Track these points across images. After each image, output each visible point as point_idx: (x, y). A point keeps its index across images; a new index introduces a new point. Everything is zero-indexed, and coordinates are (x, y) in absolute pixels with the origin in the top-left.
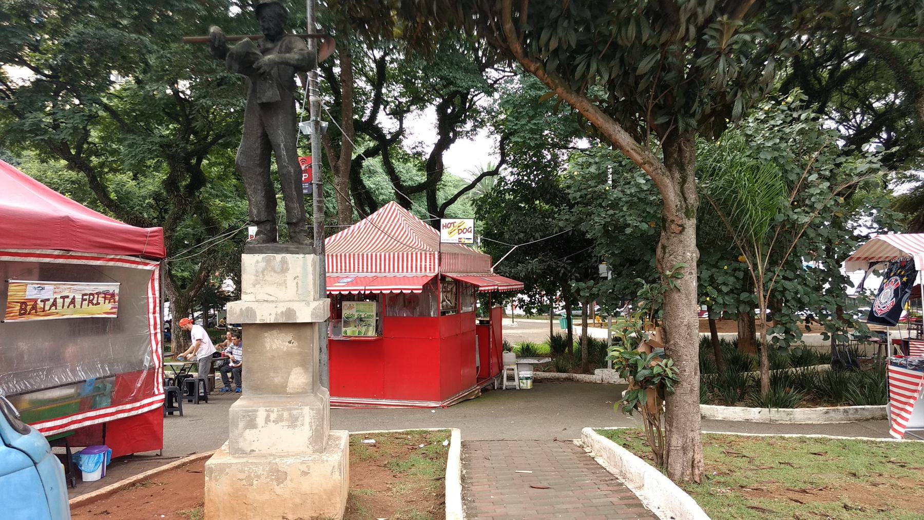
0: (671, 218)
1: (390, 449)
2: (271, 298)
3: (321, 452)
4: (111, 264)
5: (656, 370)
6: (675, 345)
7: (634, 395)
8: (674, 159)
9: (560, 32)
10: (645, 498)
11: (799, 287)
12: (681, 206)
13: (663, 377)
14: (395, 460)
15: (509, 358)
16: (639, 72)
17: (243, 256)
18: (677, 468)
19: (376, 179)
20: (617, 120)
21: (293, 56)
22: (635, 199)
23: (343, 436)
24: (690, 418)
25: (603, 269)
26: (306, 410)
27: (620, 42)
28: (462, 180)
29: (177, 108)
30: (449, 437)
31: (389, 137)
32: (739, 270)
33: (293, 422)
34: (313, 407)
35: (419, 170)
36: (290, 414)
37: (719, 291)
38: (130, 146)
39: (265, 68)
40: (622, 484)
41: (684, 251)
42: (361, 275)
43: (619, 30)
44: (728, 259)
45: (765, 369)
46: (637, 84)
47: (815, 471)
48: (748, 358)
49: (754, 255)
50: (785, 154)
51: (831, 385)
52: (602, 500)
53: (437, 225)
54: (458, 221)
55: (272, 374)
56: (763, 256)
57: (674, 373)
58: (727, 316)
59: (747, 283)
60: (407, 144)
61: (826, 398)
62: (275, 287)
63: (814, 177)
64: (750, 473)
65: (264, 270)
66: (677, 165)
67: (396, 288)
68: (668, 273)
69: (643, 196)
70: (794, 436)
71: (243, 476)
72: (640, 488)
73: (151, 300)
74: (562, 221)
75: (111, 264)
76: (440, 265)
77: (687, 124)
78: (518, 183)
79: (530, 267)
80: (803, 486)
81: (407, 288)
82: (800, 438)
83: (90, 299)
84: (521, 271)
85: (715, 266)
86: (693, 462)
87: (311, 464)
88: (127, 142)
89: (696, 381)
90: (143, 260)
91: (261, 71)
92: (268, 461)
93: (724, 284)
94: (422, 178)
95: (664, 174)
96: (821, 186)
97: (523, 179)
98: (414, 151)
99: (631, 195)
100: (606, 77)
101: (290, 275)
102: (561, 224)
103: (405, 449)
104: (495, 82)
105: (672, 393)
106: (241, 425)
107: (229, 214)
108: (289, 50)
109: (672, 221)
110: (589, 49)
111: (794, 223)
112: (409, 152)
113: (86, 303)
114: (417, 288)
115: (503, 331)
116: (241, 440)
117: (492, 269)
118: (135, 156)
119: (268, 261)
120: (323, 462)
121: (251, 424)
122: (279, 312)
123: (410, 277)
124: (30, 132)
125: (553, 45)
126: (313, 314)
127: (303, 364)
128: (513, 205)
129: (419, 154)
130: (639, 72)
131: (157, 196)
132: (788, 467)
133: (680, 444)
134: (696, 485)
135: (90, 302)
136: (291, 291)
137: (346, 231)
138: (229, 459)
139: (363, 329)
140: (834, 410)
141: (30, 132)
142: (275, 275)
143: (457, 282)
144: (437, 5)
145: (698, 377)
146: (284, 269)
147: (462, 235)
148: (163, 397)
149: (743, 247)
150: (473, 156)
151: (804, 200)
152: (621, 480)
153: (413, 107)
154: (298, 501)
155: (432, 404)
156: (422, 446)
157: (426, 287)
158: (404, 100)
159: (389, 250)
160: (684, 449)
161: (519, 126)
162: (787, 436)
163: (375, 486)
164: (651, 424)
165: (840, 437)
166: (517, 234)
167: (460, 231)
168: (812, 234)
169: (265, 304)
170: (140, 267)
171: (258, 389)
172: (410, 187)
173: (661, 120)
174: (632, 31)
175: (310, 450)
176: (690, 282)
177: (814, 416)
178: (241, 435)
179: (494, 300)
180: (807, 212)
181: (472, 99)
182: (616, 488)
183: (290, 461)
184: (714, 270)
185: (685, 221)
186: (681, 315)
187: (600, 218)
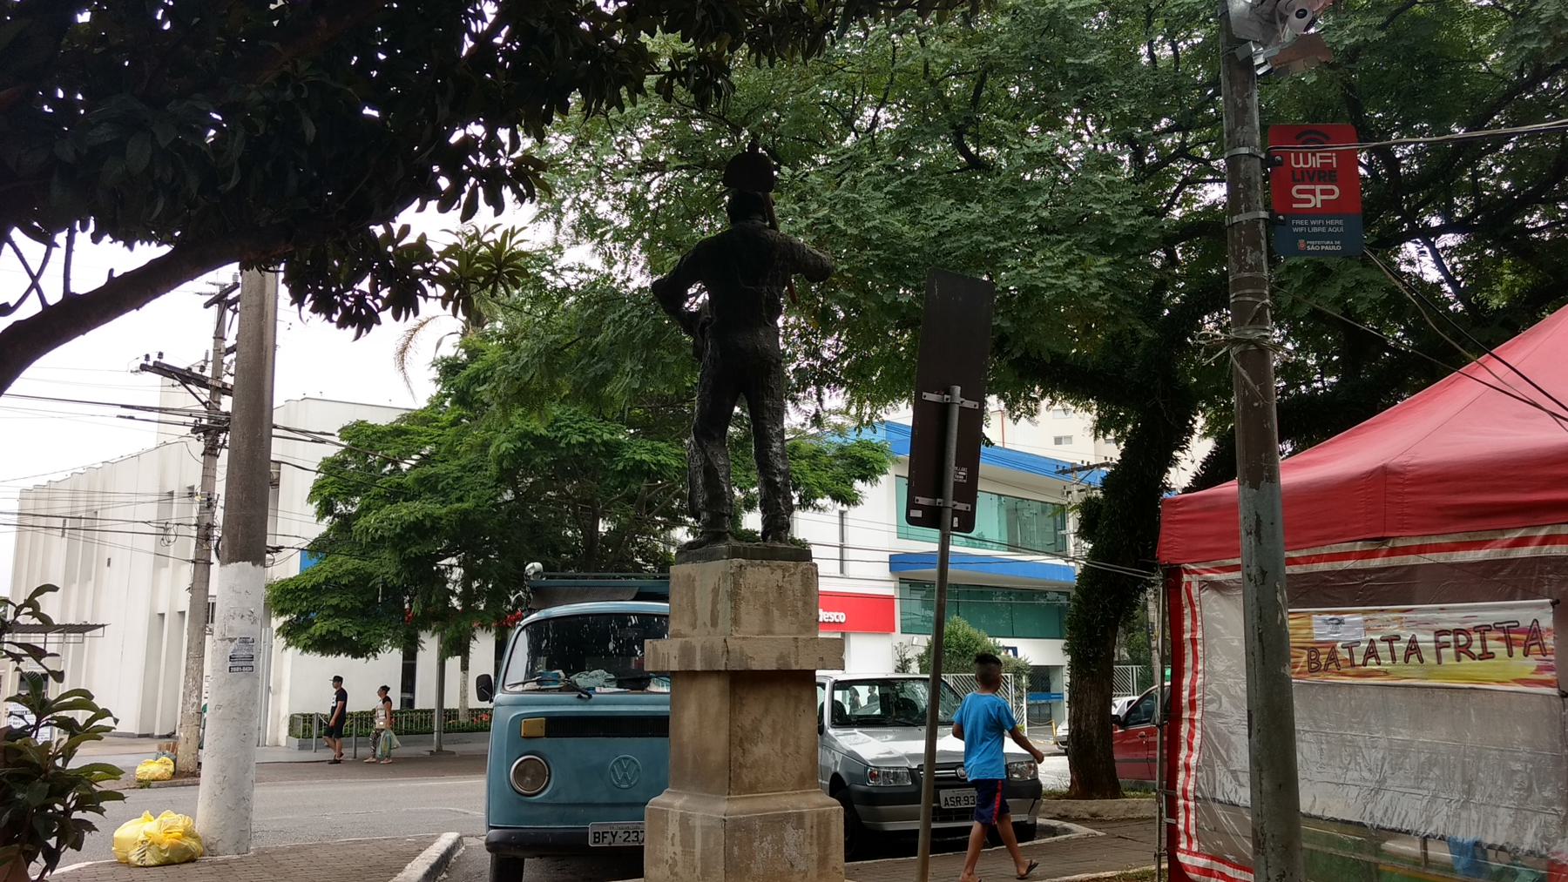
135: (1463, 650)
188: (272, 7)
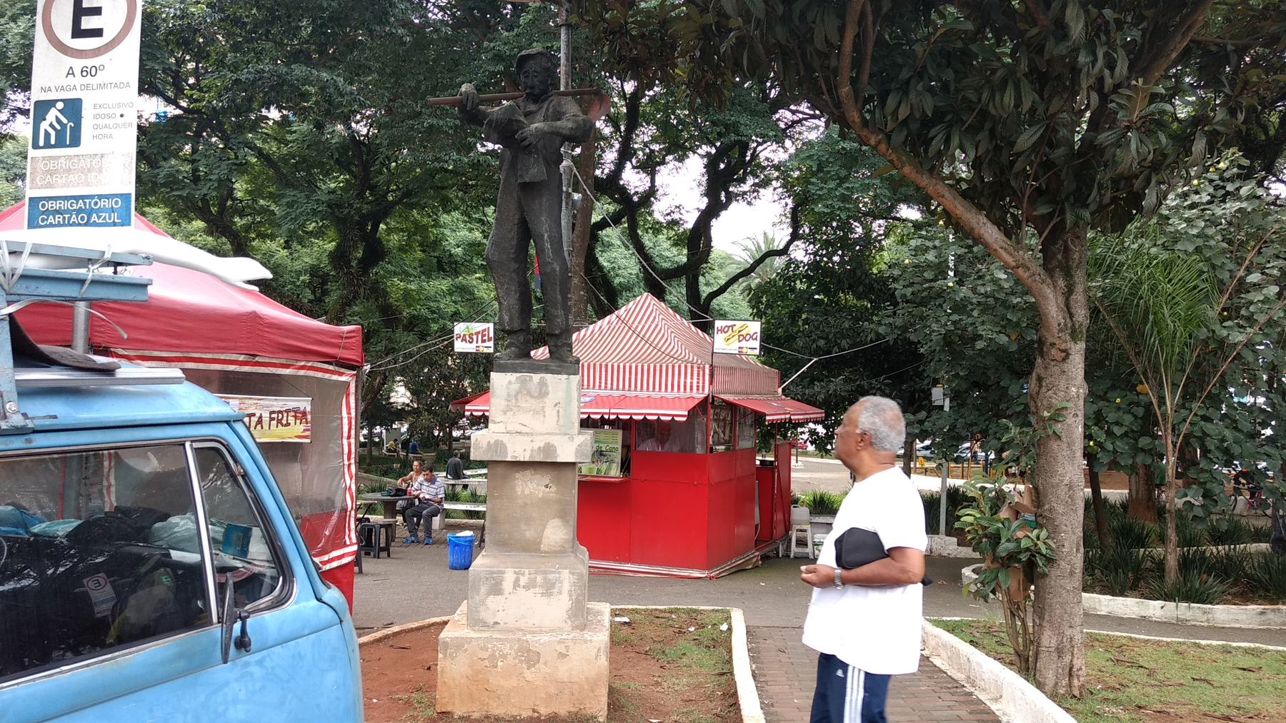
0: (1051, 340)
1: (650, 631)
2: (525, 430)
3: (582, 630)
4: (302, 373)
5: (1024, 544)
6: (1050, 510)
7: (993, 576)
8: (1056, 259)
9: (912, 96)
10: (1004, 714)
11: (1227, 433)
12: (1066, 325)
13: (1034, 552)
14: (659, 646)
15: (800, 514)
16: (1017, 148)
17: (493, 375)
18: (1050, 677)
19: (617, 257)
20: (980, 207)
21: (566, 124)
22: (991, 301)
23: (605, 608)
24: (1069, 610)
25: (937, 394)
26: (565, 574)
27: (993, 112)
28: (729, 257)
29: (357, 156)
30: (728, 619)
31: (635, 199)
32: (1138, 405)
33: (549, 589)
34: (573, 568)
35: (675, 244)
36: (545, 579)
37: (1109, 433)
38: (290, 205)
39: (531, 139)
40: (971, 694)
41: (1068, 385)
42: (603, 393)
43: (992, 97)
44: (1122, 389)
45: (1171, 546)
46: (1012, 163)
47: (1244, 692)
48: (1143, 528)
49: (1161, 385)
50: (1212, 243)
51: (1270, 574)
52: (945, 713)
53: (706, 327)
54: (739, 324)
55: (523, 527)
56: (1175, 385)
57: (1049, 547)
58: (1114, 465)
59: (1149, 421)
60: (660, 210)
61: (1261, 592)
62: (532, 418)
63: (1255, 277)
64: (1149, 690)
65: (517, 393)
66: (1062, 270)
67: (652, 413)
68: (1046, 414)
69: (1002, 296)
70: (1214, 643)
71: (485, 655)
72: (996, 700)
73: (345, 421)
74: (883, 326)
75: (302, 373)
76: (711, 383)
77: (1077, 216)
78: (814, 265)
79: (832, 387)
80: (1227, 712)
81: (666, 413)
82: (1223, 646)
83: (278, 418)
84: (819, 393)
85: (1103, 398)
86: (1071, 669)
87: (570, 644)
88: (285, 200)
89: (1078, 560)
90: (337, 369)
91: (526, 143)
92: (516, 637)
93: (1117, 423)
94: (681, 256)
95: (1043, 282)
96: (1265, 291)
97: (821, 260)
98: (669, 218)
99: (986, 295)
100: (972, 155)
101: (549, 401)
102: (881, 330)
103: (670, 631)
104: (788, 127)
105: (1044, 575)
106: (483, 589)
107: (414, 300)
108: (558, 116)
109: (1053, 345)
110: (949, 117)
111: (1221, 342)
112: (661, 219)
113: (274, 422)
114: (681, 414)
115: (793, 475)
116: (482, 608)
117: (780, 390)
118: (295, 219)
119: (523, 382)
120: (586, 641)
121: (496, 590)
122: (536, 447)
123: (670, 399)
124: (164, 185)
125: (903, 113)
126: (577, 451)
127: (562, 516)
128: (806, 296)
129: (674, 223)
130: (1017, 148)
131: (314, 271)
132: (1205, 685)
133: (1054, 643)
134: (1074, 701)
135: (279, 422)
136: (550, 422)
137: (583, 331)
138: (467, 633)
139: (604, 467)
140: (1273, 610)
141: (164, 185)
142: (532, 401)
143: (731, 406)
144: (749, 58)
145: (1080, 556)
146: (543, 393)
147: (744, 344)
148: (355, 548)
149: (1145, 373)
150: (754, 226)
151: (1238, 309)
152: (969, 689)
153: (670, 157)
154: (553, 690)
155: (696, 574)
156: (692, 629)
157: (692, 413)
158: (656, 147)
159: (646, 359)
160: (1060, 652)
161: (825, 191)
162: (1203, 642)
163: (639, 679)
164: (1013, 615)
165: (1280, 648)
166: (814, 341)
167: (743, 338)
168: (1249, 357)
169: (519, 437)
170: (335, 377)
171: (506, 545)
172: (668, 270)
173: (1043, 210)
174: (1009, 98)
175: (568, 627)
176: (1074, 426)
177: (1244, 617)
178: (483, 603)
179: (776, 434)
180: (1242, 327)
181: (755, 149)
182: (962, 698)
183: (545, 638)
184: (1101, 403)
185: (1071, 345)
186: (1061, 470)
187: (938, 325)
188: (643, 5)
